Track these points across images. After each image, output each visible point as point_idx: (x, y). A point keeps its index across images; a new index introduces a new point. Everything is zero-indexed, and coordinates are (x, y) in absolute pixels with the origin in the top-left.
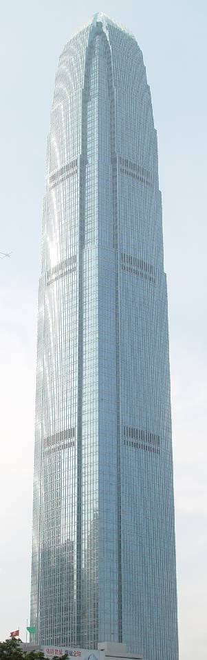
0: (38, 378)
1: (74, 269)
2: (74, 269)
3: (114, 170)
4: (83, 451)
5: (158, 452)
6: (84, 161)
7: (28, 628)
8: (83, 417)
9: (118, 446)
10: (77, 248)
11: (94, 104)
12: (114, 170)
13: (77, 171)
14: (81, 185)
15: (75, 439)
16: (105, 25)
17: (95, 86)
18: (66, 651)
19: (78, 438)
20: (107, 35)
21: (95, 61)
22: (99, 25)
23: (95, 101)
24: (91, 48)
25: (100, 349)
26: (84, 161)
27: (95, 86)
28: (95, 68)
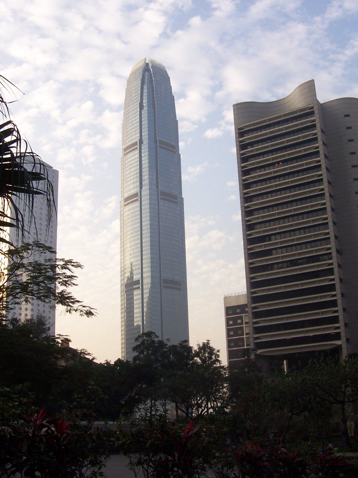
0: (123, 272)
1: (137, 200)
2: (137, 200)
3: (156, 147)
4: (142, 199)
5: (180, 289)
6: (141, 142)
7: (69, 341)
8: (143, 257)
9: (161, 288)
10: (138, 189)
11: (145, 87)
12: (156, 147)
13: (137, 148)
14: (141, 99)
15: (139, 198)
16: (150, 65)
17: (145, 101)
18: (70, 309)
19: (140, 197)
20: (152, 71)
21: (145, 87)
22: (147, 65)
23: (146, 108)
24: (144, 75)
25: (151, 241)
26: (141, 142)
27: (145, 101)
28: (145, 91)
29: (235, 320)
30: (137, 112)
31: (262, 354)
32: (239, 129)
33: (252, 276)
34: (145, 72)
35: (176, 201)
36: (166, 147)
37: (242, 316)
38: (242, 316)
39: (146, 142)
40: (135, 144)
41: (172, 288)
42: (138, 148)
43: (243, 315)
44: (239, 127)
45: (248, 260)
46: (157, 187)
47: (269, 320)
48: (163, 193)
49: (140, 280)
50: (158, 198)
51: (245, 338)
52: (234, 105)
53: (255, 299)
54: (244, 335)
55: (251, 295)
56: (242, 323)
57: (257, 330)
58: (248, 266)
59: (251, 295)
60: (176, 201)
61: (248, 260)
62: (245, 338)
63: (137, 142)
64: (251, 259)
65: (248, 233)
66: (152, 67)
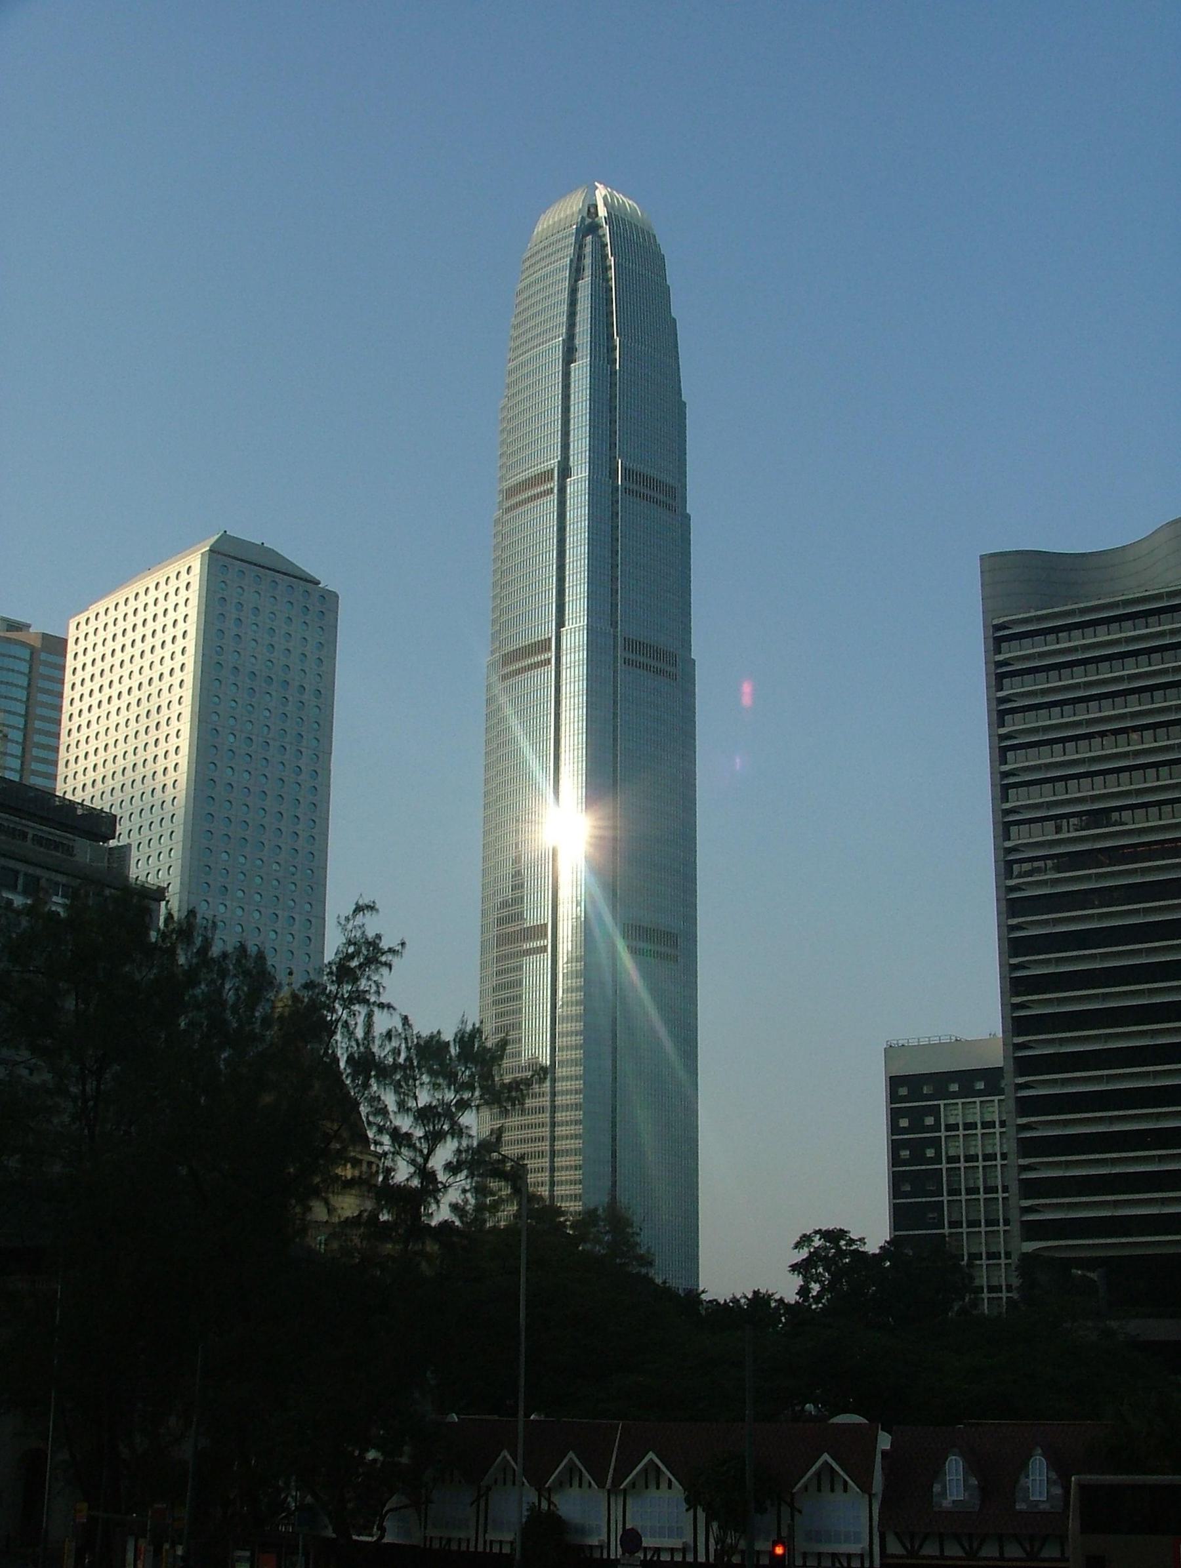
15: (554, 484)
24: (580, 246)
26: (565, 471)
29: (916, 1116)
30: (560, 303)
31: (1046, 1254)
32: (998, 628)
33: (1014, 923)
34: (584, 236)
35: (672, 669)
36: (647, 492)
37: (939, 1105)
38: (939, 1105)
39: (580, 473)
40: (546, 476)
41: (657, 502)
42: (556, 491)
43: (942, 1102)
44: (995, 622)
45: (1007, 918)
46: (614, 624)
47: (1133, 792)
48: (632, 645)
49: (556, 468)
50: (615, 658)
51: (945, 1202)
52: (982, 558)
53: (1024, 1066)
54: (941, 1164)
55: (1009, 933)
56: (936, 1127)
57: (1028, 1147)
58: (998, 781)
59: (1009, 933)
60: (672, 669)
61: (1007, 918)
62: (945, 1202)
63: (553, 470)
64: (1018, 995)
65: (1014, 961)
66: (609, 220)
